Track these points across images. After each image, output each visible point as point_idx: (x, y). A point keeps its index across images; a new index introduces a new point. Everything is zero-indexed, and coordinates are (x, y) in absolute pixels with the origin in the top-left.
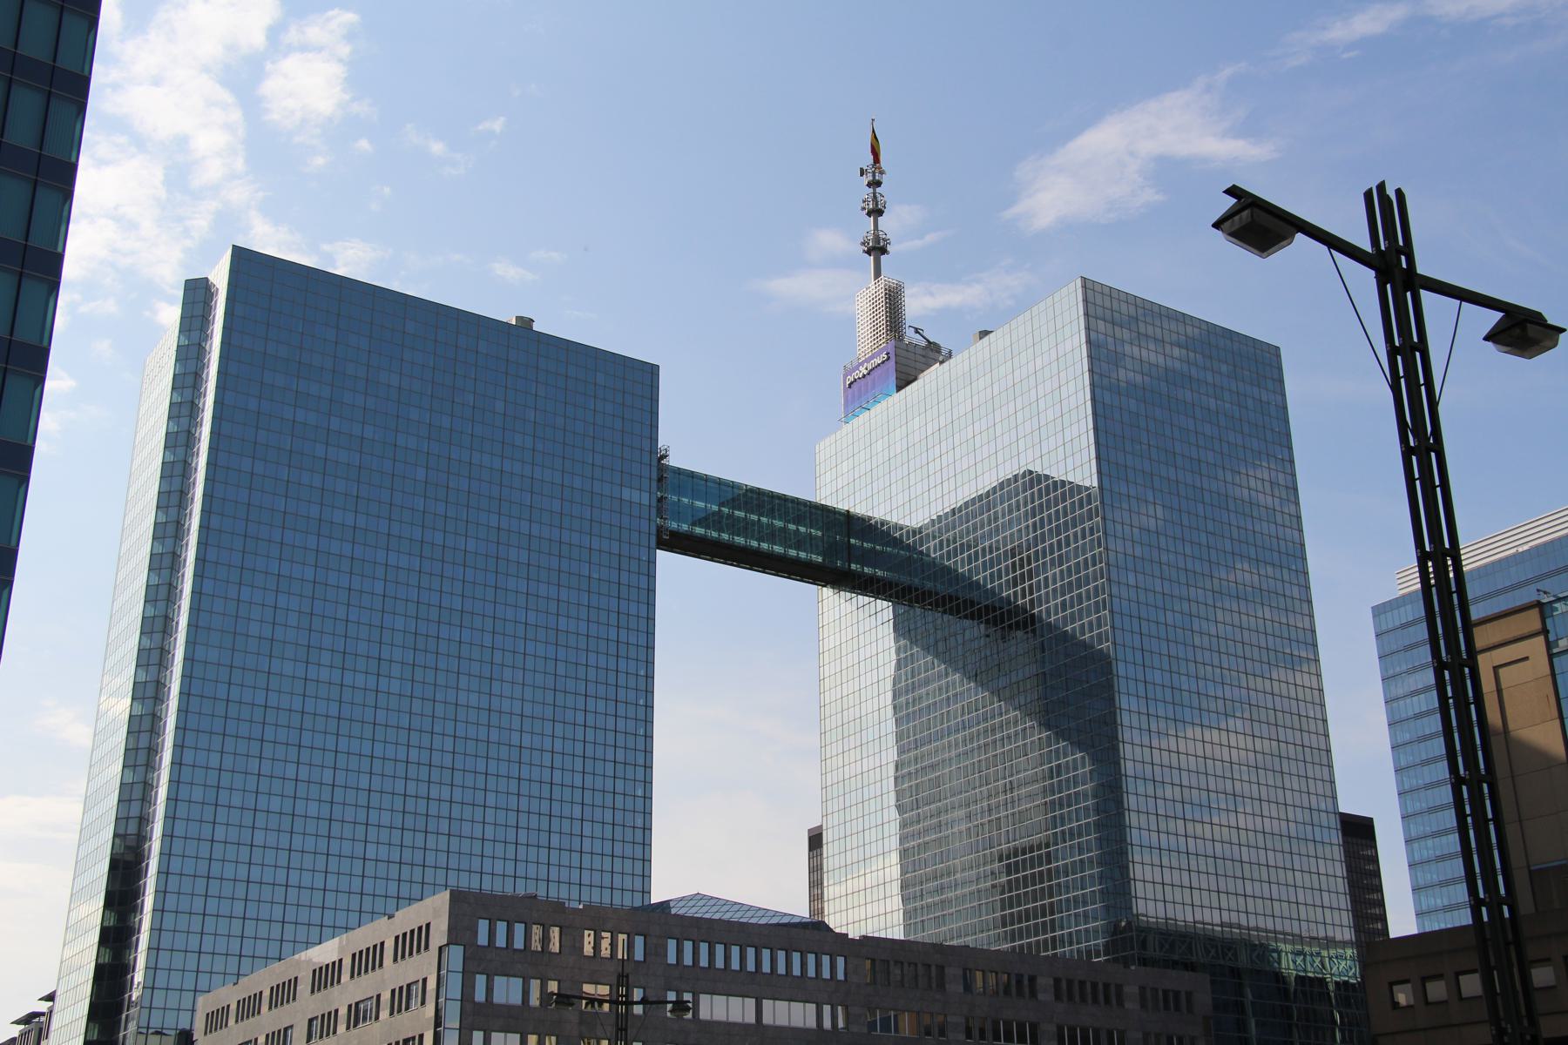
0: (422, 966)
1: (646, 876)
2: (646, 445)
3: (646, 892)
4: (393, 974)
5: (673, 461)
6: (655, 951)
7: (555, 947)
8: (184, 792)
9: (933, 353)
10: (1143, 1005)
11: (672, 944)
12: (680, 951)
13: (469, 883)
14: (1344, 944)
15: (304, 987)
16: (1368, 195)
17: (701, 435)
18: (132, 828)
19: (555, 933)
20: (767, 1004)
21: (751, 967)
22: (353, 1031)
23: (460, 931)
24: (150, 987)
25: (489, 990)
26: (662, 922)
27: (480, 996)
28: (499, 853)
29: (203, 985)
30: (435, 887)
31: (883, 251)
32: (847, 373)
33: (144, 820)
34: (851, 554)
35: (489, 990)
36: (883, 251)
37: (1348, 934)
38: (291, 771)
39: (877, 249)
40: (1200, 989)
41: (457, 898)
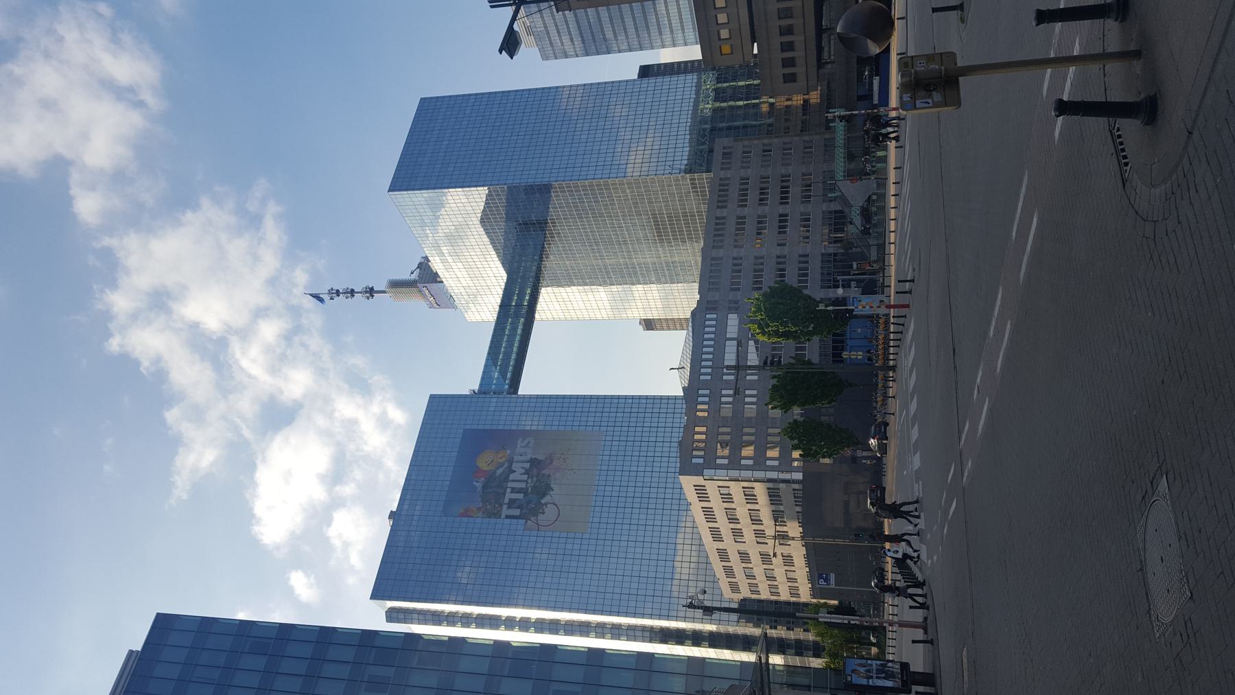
0: (712, 488)
3: (676, 398)
5: (476, 387)
6: (705, 385)
9: (424, 266)
10: (729, 169)
12: (704, 396)
13: (675, 464)
14: (699, 79)
15: (721, 545)
17: (465, 377)
23: (697, 471)
25: (723, 457)
33: (644, 629)
34: (519, 305)
38: (621, 561)
39: (371, 292)
40: (721, 143)
41: (683, 472)
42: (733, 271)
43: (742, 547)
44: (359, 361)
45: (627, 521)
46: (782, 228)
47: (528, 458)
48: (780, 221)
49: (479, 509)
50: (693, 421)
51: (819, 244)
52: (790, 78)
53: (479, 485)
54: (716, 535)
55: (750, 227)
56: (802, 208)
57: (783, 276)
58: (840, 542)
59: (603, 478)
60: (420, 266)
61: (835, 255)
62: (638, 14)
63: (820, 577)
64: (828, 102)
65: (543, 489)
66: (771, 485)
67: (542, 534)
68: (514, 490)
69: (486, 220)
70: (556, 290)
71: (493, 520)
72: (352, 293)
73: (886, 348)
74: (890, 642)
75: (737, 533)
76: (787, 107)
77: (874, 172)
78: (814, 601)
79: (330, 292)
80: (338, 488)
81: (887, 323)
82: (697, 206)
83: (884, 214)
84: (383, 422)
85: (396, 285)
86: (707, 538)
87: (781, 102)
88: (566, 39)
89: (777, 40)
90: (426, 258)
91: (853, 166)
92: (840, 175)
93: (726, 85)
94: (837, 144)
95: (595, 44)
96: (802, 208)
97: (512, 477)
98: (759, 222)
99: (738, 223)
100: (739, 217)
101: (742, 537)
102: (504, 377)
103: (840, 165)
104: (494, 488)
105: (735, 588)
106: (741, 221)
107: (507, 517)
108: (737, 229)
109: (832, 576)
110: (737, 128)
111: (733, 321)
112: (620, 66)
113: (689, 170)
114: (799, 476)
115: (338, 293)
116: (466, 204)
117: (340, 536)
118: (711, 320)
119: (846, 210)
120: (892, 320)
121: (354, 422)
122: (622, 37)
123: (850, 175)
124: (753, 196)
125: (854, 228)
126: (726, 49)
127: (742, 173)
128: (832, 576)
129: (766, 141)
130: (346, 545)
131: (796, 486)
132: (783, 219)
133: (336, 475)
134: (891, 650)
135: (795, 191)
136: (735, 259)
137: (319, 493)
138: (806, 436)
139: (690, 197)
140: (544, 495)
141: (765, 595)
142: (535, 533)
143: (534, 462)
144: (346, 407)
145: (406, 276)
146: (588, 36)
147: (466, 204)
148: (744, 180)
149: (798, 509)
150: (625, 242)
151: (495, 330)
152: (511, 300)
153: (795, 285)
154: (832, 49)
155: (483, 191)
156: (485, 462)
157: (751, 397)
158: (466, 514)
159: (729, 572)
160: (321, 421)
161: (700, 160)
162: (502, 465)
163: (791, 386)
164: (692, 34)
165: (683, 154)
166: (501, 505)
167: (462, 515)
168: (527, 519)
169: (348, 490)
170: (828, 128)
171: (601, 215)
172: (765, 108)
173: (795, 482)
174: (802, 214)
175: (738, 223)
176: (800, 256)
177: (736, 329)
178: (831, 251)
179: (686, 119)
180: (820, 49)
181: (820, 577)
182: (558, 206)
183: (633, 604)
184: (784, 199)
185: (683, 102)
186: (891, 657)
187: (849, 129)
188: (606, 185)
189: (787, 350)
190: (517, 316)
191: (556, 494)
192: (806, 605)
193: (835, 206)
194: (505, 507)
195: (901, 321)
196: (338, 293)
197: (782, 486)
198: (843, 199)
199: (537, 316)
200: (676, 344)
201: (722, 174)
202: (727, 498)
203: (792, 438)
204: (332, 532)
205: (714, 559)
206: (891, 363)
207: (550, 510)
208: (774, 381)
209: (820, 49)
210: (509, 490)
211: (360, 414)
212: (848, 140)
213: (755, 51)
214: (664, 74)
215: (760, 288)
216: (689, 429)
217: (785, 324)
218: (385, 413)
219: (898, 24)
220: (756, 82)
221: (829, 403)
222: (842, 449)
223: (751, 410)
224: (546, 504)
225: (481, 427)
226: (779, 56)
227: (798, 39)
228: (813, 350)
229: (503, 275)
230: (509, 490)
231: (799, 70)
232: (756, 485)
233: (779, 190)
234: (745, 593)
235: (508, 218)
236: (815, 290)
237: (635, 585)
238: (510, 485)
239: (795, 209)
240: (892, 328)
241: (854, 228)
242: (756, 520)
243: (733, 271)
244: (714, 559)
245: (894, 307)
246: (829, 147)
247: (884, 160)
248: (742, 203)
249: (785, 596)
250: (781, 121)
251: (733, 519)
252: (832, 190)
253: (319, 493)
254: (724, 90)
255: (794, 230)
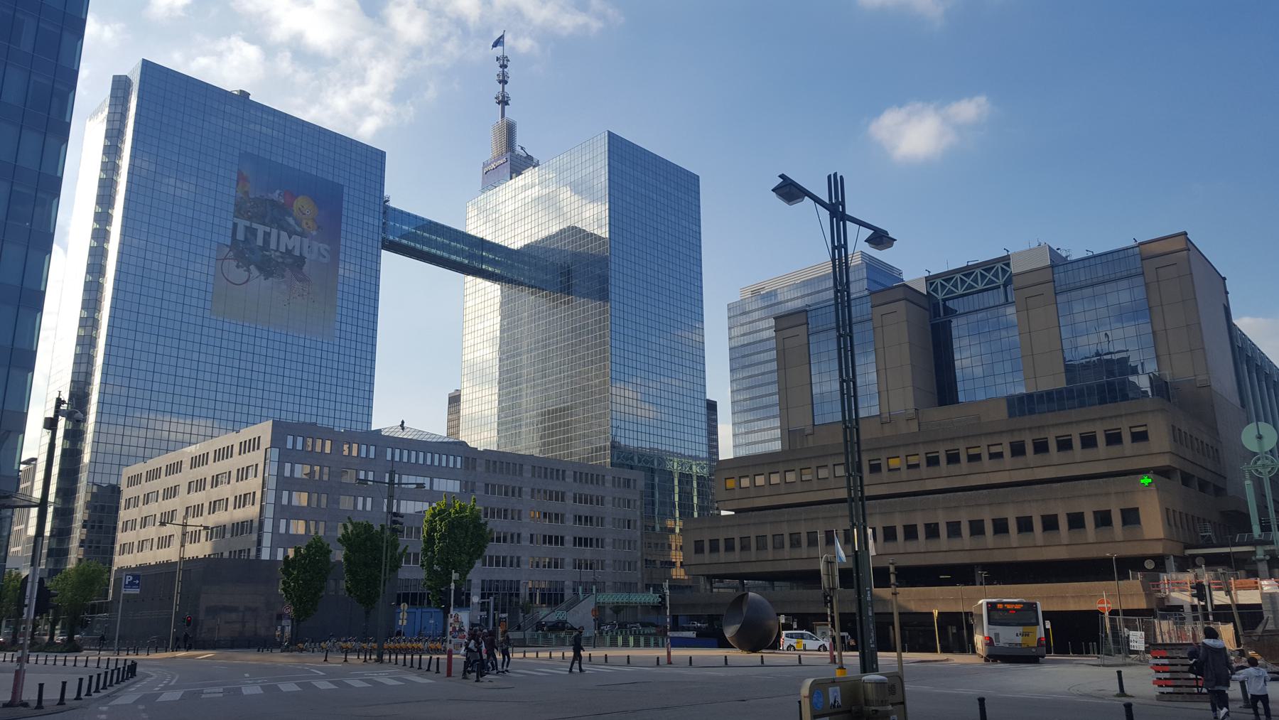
0: (256, 457)
1: (370, 415)
2: (378, 193)
3: (369, 423)
4: (238, 462)
5: (392, 204)
6: (380, 454)
7: (328, 450)
8: (113, 361)
11: (389, 451)
14: (703, 459)
15: (186, 466)
16: (829, 177)
17: (405, 192)
18: (82, 378)
19: (328, 443)
20: (435, 480)
21: (429, 462)
22: (215, 489)
23: (277, 440)
24: (93, 461)
25: (292, 471)
26: (378, 439)
27: (287, 473)
28: (291, 400)
29: (124, 461)
30: (267, 418)
31: (507, 103)
32: (485, 165)
33: (89, 374)
34: (483, 260)
35: (292, 471)
36: (507, 103)
37: (705, 455)
39: (503, 101)
40: (640, 479)
42: (506, 487)
43: (183, 489)
44: (431, 93)
45: (223, 361)
46: (549, 539)
47: (306, 254)
48: (557, 538)
49: (246, 193)
50: (338, 439)
51: (529, 578)
52: (699, 547)
53: (275, 196)
54: (197, 461)
55: (554, 507)
56: (568, 560)
57: (498, 540)
58: (176, 599)
59: (277, 337)
60: (529, 158)
61: (517, 595)
62: (766, 401)
63: (136, 577)
64: (676, 586)
65: (268, 268)
66: (256, 524)
67: (213, 262)
68: (267, 235)
69: (574, 231)
70: (498, 300)
71: (232, 208)
72: (503, 82)
73: (405, 651)
74: (51, 657)
75: (199, 485)
76: (670, 546)
77: (601, 634)
78: (115, 568)
79: (505, 58)
80: (288, 54)
81: (437, 651)
82: (578, 452)
83: (556, 645)
84: (362, 111)
85: (510, 130)
86: (193, 450)
87: (676, 540)
88: (746, 329)
89: (736, 534)
90: (537, 165)
91: (608, 612)
92: (602, 598)
93: (695, 485)
94: (632, 595)
95: (740, 358)
96: (568, 560)
97: (284, 234)
98: (557, 515)
99: (557, 493)
100: (563, 494)
101: (196, 493)
102: (402, 237)
103: (609, 598)
104: (276, 214)
105: (134, 480)
106: (560, 497)
107: (235, 225)
108: (551, 492)
109: (137, 591)
110: (653, 495)
111: (453, 486)
112: (719, 384)
113: (614, 446)
114: (265, 555)
115: (504, 66)
116: (593, 217)
117: (231, 50)
118: (455, 462)
119: (564, 605)
120: (435, 657)
121: (363, 81)
122: (746, 383)
123: (600, 608)
124: (585, 510)
125: (546, 614)
126: (731, 484)
127: (608, 499)
128: (137, 591)
129: (638, 524)
130: (220, 55)
131: (253, 553)
132: (559, 540)
133: (302, 54)
134: (42, 658)
135: (587, 553)
136: (520, 489)
137: (279, 34)
138: (309, 566)
139: (586, 445)
140: (260, 268)
141: (124, 515)
142: (214, 254)
143: (301, 260)
144: (381, 73)
145: (520, 141)
146: (747, 351)
147: (593, 217)
148: (600, 501)
149: (226, 555)
150: (544, 376)
151: (456, 231)
152: (489, 251)
153: (487, 552)
154: (725, 590)
155: (604, 232)
156: (303, 205)
157: (365, 504)
158: (241, 178)
159: (154, 475)
160: (366, 45)
161: (623, 457)
162: (299, 224)
163: (371, 548)
164: (743, 452)
165: (629, 441)
166: (249, 219)
167: (240, 174)
168: (231, 248)
169: (284, 64)
170: (647, 587)
171: (574, 352)
172: (670, 523)
173: (259, 551)
174: (563, 560)
175: (557, 493)
176: (518, 558)
177: (443, 489)
178: (522, 591)
179: (664, 445)
180: (722, 577)
181: (136, 577)
182: (586, 308)
183: (120, 362)
184: (579, 541)
185: (680, 445)
186: (32, 659)
187: (647, 608)
188: (605, 359)
189: (413, 543)
190: (471, 256)
191: (259, 283)
192: (111, 562)
193: (568, 593)
194: (248, 223)
195: (433, 668)
196: (504, 66)
197: (255, 537)
198: (576, 601)
199: (470, 278)
200: (433, 425)
201: (609, 478)
202: (243, 474)
203: (308, 547)
204: (236, 42)
205: (171, 458)
206: (386, 657)
207: (241, 274)
208: (377, 528)
209: (722, 577)
210: (268, 229)
211: (370, 89)
212: (634, 607)
213: (723, 513)
214: (709, 425)
215: (486, 515)
216: (328, 433)
217: (442, 538)
218: (372, 113)
219: (755, 657)
220: (696, 515)
221: (348, 589)
222: (293, 603)
223: (346, 503)
224: (248, 270)
225: (345, 205)
226: (721, 536)
227: (736, 556)
228: (412, 573)
229: (516, 243)
230: (268, 229)
231: (707, 557)
232: (257, 508)
233: (589, 536)
234: (127, 493)
235: (575, 255)
236: (478, 574)
237: (143, 366)
238: (274, 232)
239: (568, 553)
240: (426, 657)
241: (546, 614)
242: (214, 506)
243: (506, 487)
244: (171, 458)
245: (450, 659)
246: (628, 587)
247: (614, 644)
248: (578, 498)
249: (122, 537)
250: (659, 540)
251: (216, 481)
252: (585, 591)
253: (279, 34)
254: (690, 483)
255: (547, 552)
